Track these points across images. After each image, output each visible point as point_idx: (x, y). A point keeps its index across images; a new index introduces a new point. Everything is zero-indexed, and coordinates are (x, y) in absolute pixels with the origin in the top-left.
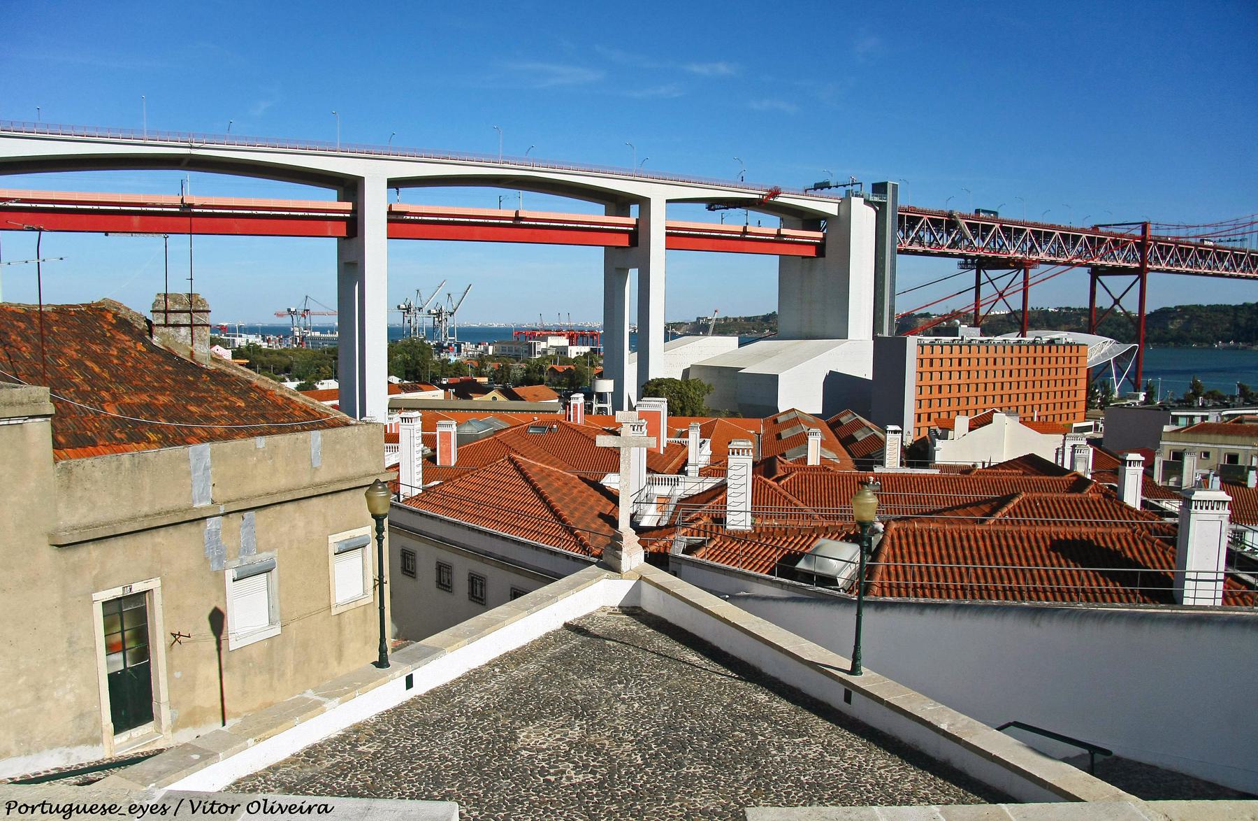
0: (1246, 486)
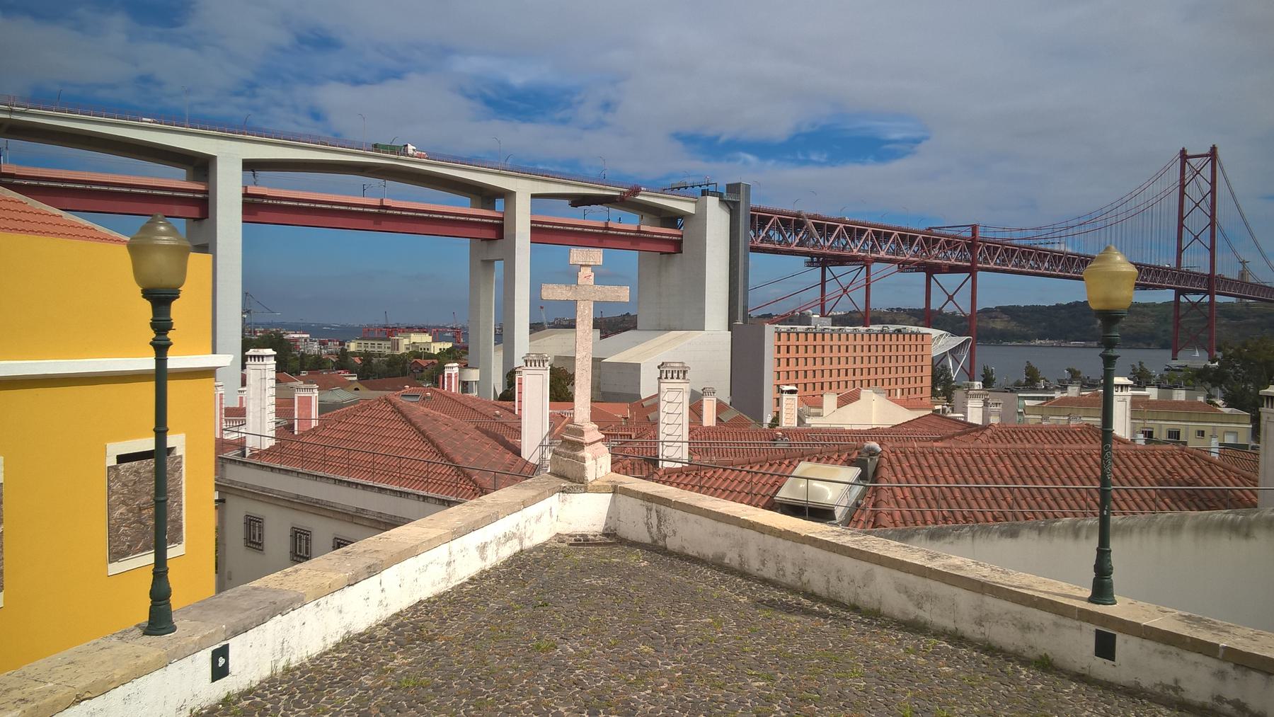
0: (517, 452)
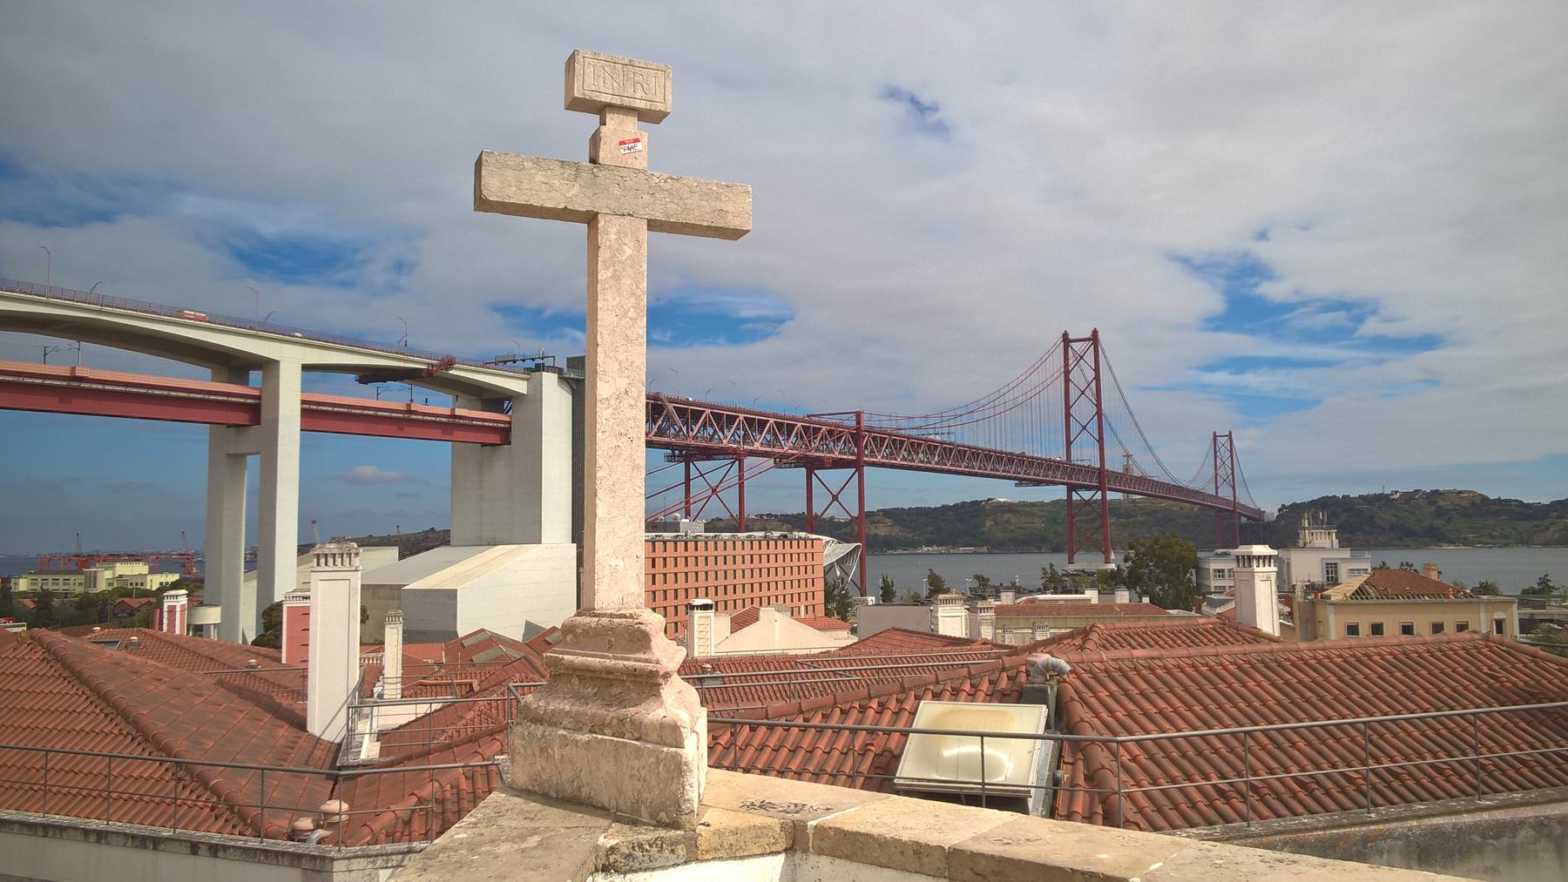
0: (300, 723)
